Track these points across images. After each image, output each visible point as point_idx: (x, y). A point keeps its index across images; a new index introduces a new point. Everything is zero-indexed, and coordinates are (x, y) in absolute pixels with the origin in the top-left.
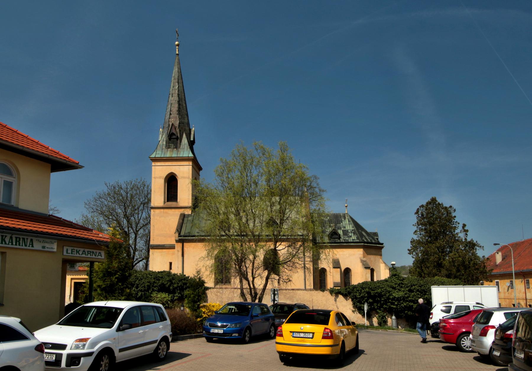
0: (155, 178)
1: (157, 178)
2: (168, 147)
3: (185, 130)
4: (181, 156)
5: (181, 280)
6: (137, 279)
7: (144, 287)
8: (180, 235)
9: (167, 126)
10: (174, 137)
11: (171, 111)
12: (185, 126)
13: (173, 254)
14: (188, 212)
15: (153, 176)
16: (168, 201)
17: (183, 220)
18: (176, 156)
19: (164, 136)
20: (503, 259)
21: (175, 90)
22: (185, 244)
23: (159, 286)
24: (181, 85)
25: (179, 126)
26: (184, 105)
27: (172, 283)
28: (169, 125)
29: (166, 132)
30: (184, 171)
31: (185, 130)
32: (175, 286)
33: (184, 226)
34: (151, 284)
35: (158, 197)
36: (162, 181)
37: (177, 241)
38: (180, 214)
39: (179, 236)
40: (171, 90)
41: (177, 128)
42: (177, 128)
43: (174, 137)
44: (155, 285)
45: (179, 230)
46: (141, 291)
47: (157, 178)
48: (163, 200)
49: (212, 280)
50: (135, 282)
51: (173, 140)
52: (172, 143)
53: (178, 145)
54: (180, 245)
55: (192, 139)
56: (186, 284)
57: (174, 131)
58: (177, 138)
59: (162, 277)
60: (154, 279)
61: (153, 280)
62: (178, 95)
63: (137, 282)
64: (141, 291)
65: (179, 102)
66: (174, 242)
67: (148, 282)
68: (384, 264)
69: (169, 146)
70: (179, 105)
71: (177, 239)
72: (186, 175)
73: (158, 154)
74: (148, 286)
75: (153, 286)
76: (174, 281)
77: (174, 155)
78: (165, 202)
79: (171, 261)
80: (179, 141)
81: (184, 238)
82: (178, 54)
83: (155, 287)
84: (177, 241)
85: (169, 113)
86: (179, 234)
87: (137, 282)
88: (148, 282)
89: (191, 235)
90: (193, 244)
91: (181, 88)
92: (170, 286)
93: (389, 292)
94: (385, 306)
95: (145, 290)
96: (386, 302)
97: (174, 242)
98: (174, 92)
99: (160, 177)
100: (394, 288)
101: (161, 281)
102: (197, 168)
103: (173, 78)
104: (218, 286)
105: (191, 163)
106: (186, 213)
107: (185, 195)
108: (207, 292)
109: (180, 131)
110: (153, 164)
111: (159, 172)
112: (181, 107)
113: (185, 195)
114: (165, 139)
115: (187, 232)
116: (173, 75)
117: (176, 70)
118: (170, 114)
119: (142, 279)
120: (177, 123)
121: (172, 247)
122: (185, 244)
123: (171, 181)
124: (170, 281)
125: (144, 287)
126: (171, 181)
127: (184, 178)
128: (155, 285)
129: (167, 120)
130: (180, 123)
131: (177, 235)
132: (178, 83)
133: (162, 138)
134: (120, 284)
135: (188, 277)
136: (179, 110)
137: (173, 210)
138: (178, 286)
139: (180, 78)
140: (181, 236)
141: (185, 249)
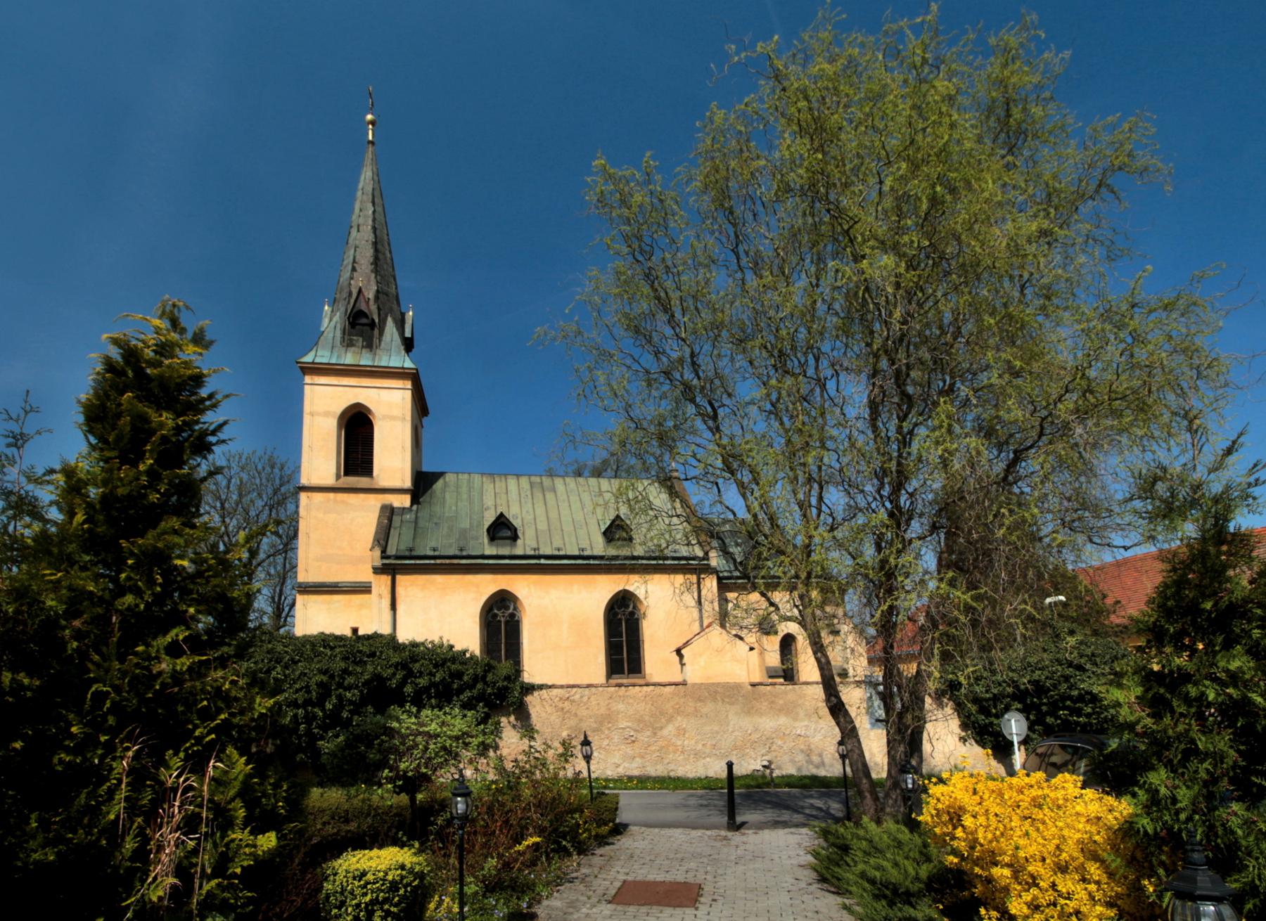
0: (312, 414)
1: (319, 414)
2: (348, 344)
3: (391, 311)
5: (445, 661)
6: (278, 661)
7: (307, 688)
8: (384, 555)
9: (345, 295)
10: (364, 321)
11: (354, 261)
12: (389, 300)
13: (361, 606)
14: (404, 501)
15: (307, 407)
16: (347, 473)
17: (390, 520)
18: (370, 363)
19: (337, 318)
21: (365, 216)
22: (398, 577)
23: (366, 683)
24: (379, 209)
25: (377, 298)
27: (410, 674)
28: (350, 294)
29: (343, 309)
30: (390, 406)
31: (391, 311)
32: (423, 682)
33: (394, 534)
34: (332, 677)
35: (319, 457)
37: (377, 571)
38: (379, 506)
39: (382, 558)
40: (354, 217)
41: (372, 302)
42: (372, 302)
43: (364, 321)
44: (350, 680)
45: (383, 538)
46: (294, 704)
47: (319, 414)
48: (334, 470)
50: (268, 671)
51: (361, 327)
53: (376, 341)
54: (386, 580)
55: (408, 334)
56: (459, 675)
57: (363, 307)
58: (372, 325)
59: (373, 655)
60: (345, 659)
61: (343, 665)
62: (374, 229)
63: (277, 672)
64: (294, 704)
65: (375, 244)
66: (364, 574)
67: (321, 672)
69: (351, 340)
70: (376, 250)
71: (378, 563)
72: (396, 412)
73: (321, 356)
74: (320, 685)
75: (340, 685)
76: (416, 667)
77: (365, 360)
78: (338, 477)
79: (355, 625)
80: (376, 332)
81: (397, 563)
82: (372, 143)
83: (349, 688)
84: (377, 571)
85: (350, 267)
86: (383, 552)
87: (277, 672)
88: (321, 672)
89: (414, 553)
91: (380, 217)
92: (403, 683)
93: (1067, 678)
94: (1049, 720)
95: (308, 702)
96: (1054, 708)
97: (364, 574)
98: (361, 221)
99: (327, 414)
100: (1080, 668)
101: (370, 668)
103: (359, 193)
104: (612, 681)
105: (409, 384)
106: (396, 504)
107: (393, 459)
108: (528, 699)
109: (379, 309)
110: (308, 379)
111: (324, 402)
112: (381, 256)
113: (393, 459)
114: (339, 326)
115: (402, 547)
116: (360, 186)
118: (354, 269)
119: (295, 663)
120: (370, 294)
122: (398, 577)
123: (357, 429)
124: (403, 665)
125: (307, 688)
126: (357, 429)
128: (350, 680)
129: (346, 284)
130: (378, 291)
131: (377, 553)
133: (331, 321)
135: (464, 652)
136: (376, 262)
137: (362, 496)
138: (433, 684)
139: (377, 193)
140: (388, 557)
141: (400, 590)
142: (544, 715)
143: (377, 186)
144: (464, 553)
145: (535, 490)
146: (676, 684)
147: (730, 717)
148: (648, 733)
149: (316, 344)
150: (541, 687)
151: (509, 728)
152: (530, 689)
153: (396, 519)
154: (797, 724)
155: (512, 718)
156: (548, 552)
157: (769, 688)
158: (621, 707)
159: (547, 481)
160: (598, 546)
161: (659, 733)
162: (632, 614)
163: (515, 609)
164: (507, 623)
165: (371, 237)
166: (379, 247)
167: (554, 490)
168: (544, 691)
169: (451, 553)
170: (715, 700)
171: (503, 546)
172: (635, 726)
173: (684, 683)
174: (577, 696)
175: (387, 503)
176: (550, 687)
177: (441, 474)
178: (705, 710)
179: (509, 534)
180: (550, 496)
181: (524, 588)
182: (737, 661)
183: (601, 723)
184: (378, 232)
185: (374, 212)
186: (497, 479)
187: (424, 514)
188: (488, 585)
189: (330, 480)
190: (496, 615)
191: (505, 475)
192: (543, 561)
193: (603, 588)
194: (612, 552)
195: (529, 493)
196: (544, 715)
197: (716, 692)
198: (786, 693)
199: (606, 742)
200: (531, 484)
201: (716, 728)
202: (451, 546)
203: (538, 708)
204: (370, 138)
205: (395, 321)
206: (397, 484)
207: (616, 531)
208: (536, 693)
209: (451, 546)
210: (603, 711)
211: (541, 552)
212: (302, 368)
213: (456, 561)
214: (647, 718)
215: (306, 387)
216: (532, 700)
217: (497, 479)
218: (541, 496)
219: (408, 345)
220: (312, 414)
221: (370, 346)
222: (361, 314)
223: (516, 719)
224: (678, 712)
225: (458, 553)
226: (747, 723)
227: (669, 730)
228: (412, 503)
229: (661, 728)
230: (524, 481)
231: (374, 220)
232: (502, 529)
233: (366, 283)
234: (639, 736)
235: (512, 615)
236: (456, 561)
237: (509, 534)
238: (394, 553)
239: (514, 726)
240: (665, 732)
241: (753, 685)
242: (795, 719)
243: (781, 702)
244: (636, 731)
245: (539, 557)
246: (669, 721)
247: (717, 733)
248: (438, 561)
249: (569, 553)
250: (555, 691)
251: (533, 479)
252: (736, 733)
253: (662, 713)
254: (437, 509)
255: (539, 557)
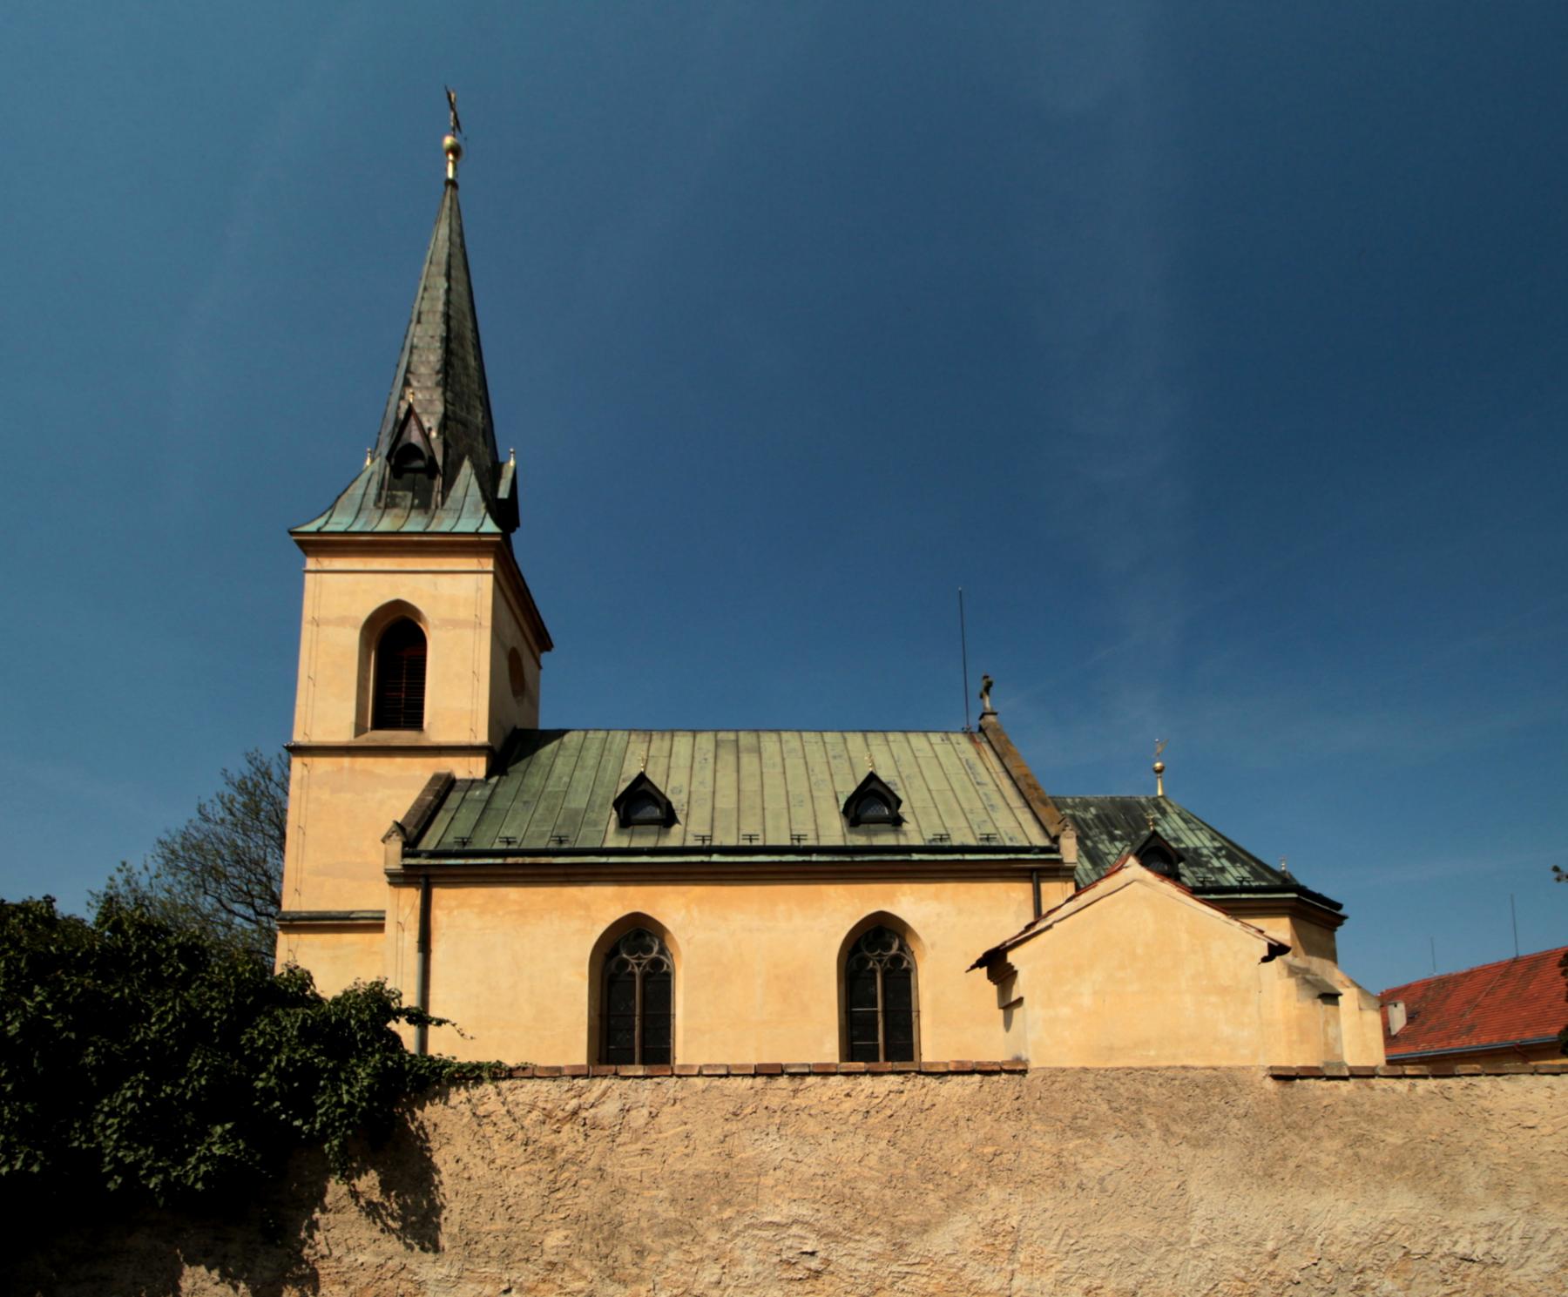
1: (328, 622)
2: (386, 502)
3: (471, 452)
4: (445, 528)
8: (410, 846)
10: (419, 464)
11: (408, 370)
12: (472, 427)
14: (477, 767)
15: (308, 613)
16: (379, 724)
20: (1411, 1018)
21: (433, 299)
24: (460, 288)
25: (443, 427)
26: (472, 362)
30: (457, 605)
33: (442, 819)
35: (329, 695)
36: (351, 639)
37: (399, 879)
38: (428, 776)
39: (405, 855)
43: (419, 464)
45: (411, 833)
47: (328, 622)
49: (455, 1217)
51: (412, 471)
52: (404, 488)
54: (412, 896)
57: (415, 437)
58: (431, 469)
62: (447, 317)
65: (447, 341)
68: (1354, 990)
69: (393, 497)
71: (396, 864)
72: (464, 613)
77: (415, 524)
78: (360, 729)
80: (438, 482)
82: (453, 184)
90: (478, 895)
98: (425, 306)
99: (342, 621)
102: (515, 596)
105: (488, 564)
107: (458, 696)
108: (431, 1113)
109: (446, 445)
110: (311, 563)
111: (339, 603)
112: (456, 362)
113: (458, 696)
117: (443, 231)
120: (431, 422)
121: (373, 923)
122: (437, 893)
123: (396, 645)
126: (396, 645)
127: (455, 624)
130: (446, 417)
131: (396, 846)
132: (448, 277)
134: (258, 1157)
136: (449, 343)
137: (400, 761)
139: (457, 262)
141: (438, 915)
142: (480, 1170)
143: (457, 251)
144: (565, 846)
145: (722, 752)
146: (987, 1072)
147: (1194, 1189)
148: (875, 1245)
149: (332, 507)
150: (472, 1074)
151: (353, 1213)
152: (439, 1078)
153: (454, 798)
154: (1456, 1218)
155: (369, 1183)
156: (731, 841)
157: (1346, 1087)
158: (773, 1148)
159: (746, 739)
160: (834, 831)
161: (917, 1247)
162: (897, 960)
163: (663, 950)
164: (645, 977)
165: (440, 330)
166: (454, 345)
167: (759, 751)
168: (488, 1088)
169: (541, 844)
170: (1135, 1128)
171: (641, 834)
172: (825, 1218)
173: (1017, 1069)
174: (610, 1109)
175: (444, 770)
176: (511, 1074)
177: (560, 734)
178: (1092, 1167)
179: (657, 813)
180: (749, 761)
181: (672, 907)
182: (1224, 991)
183: (693, 1204)
184: (453, 323)
185: (448, 291)
186: (656, 736)
187: (509, 785)
188: (607, 905)
189: (341, 730)
190: (625, 963)
191: (673, 731)
192: (716, 858)
193: (842, 908)
194: (860, 840)
195: (710, 756)
196: (480, 1170)
197: (1139, 1100)
198: (1415, 1107)
199: (711, 1273)
200: (717, 744)
201: (1140, 1231)
202: (543, 835)
203: (459, 1148)
204: (450, 175)
205: (476, 466)
206: (463, 738)
207: (872, 801)
208: (458, 1096)
209: (543, 835)
210: (704, 1161)
211: (716, 843)
212: (301, 544)
213: (543, 860)
214: (870, 1190)
215: (308, 577)
216: (446, 1122)
217: (656, 736)
218: (731, 759)
219: (506, 513)
220: (316, 622)
221: (424, 505)
222: (413, 451)
223: (385, 1187)
224: (991, 1168)
225: (553, 845)
226: (1261, 1213)
227: (955, 1236)
228: (490, 773)
229: (925, 1228)
230: (706, 741)
231: (448, 303)
232: (641, 802)
233: (428, 404)
234: (838, 1253)
235: (657, 964)
236: (543, 860)
237: (657, 813)
238: (431, 847)
239: (372, 1210)
240: (939, 1242)
241: (1284, 1077)
242: (1452, 1199)
243: (1395, 1138)
244: (824, 1234)
245: (709, 851)
246: (959, 1198)
247: (1144, 1247)
248: (510, 860)
249: (771, 842)
250: (527, 1090)
251: (721, 735)
252: (1219, 1251)
253: (928, 1175)
254: (535, 781)
255: (709, 851)
